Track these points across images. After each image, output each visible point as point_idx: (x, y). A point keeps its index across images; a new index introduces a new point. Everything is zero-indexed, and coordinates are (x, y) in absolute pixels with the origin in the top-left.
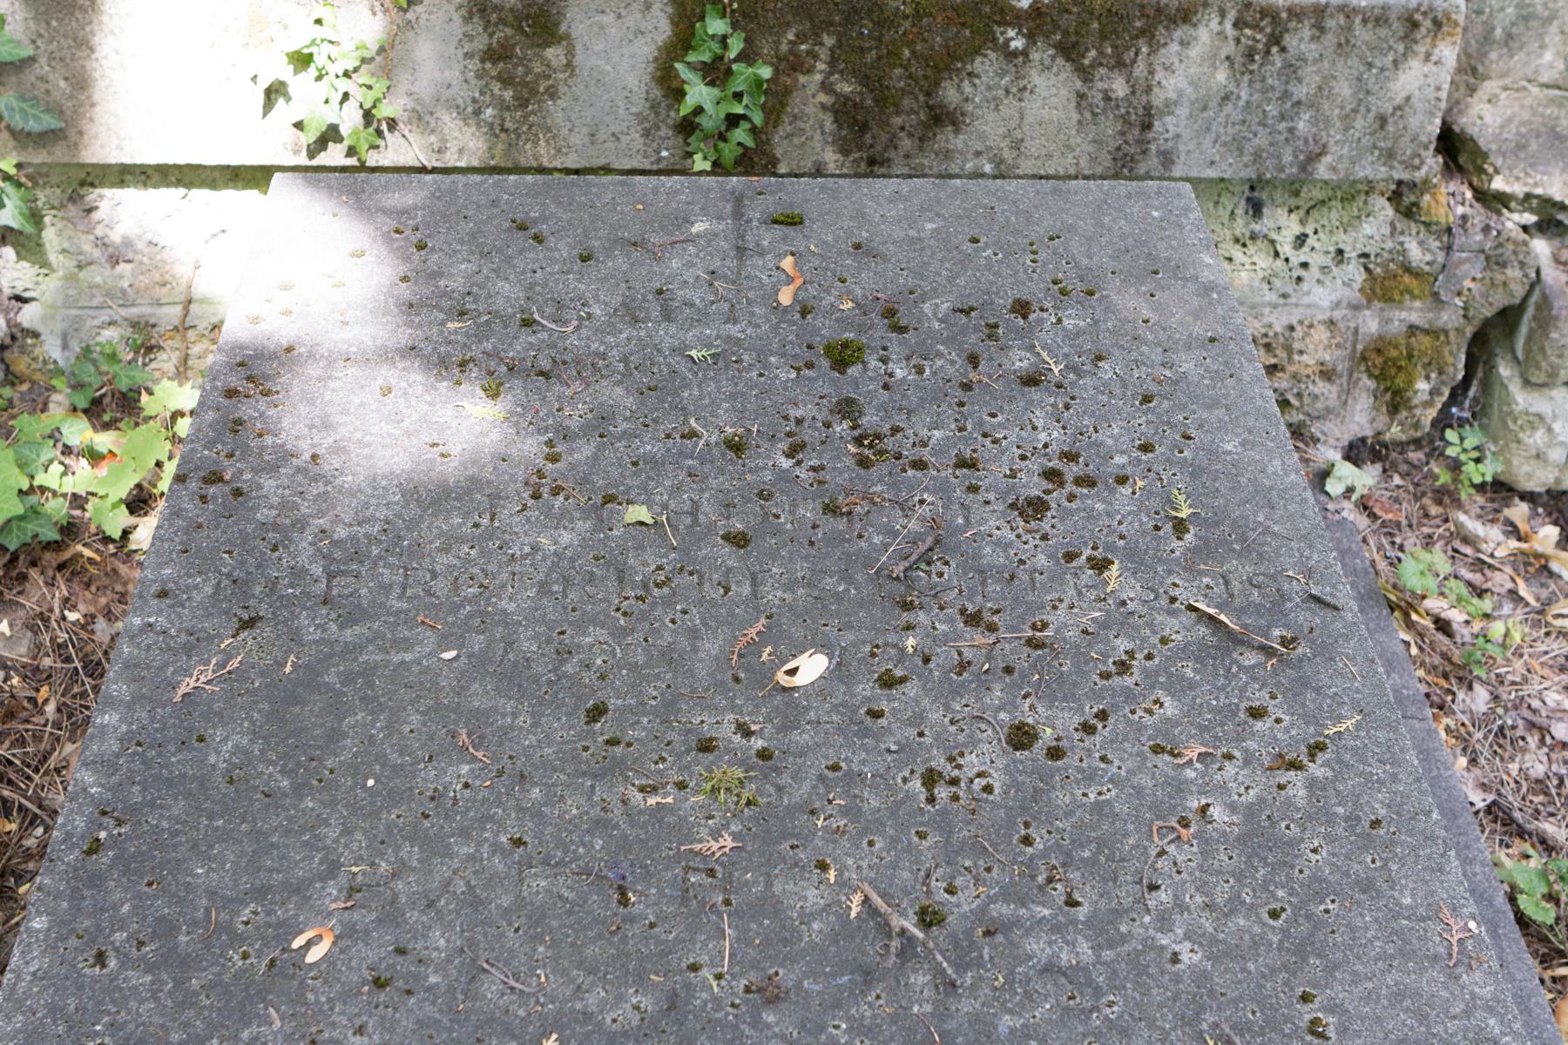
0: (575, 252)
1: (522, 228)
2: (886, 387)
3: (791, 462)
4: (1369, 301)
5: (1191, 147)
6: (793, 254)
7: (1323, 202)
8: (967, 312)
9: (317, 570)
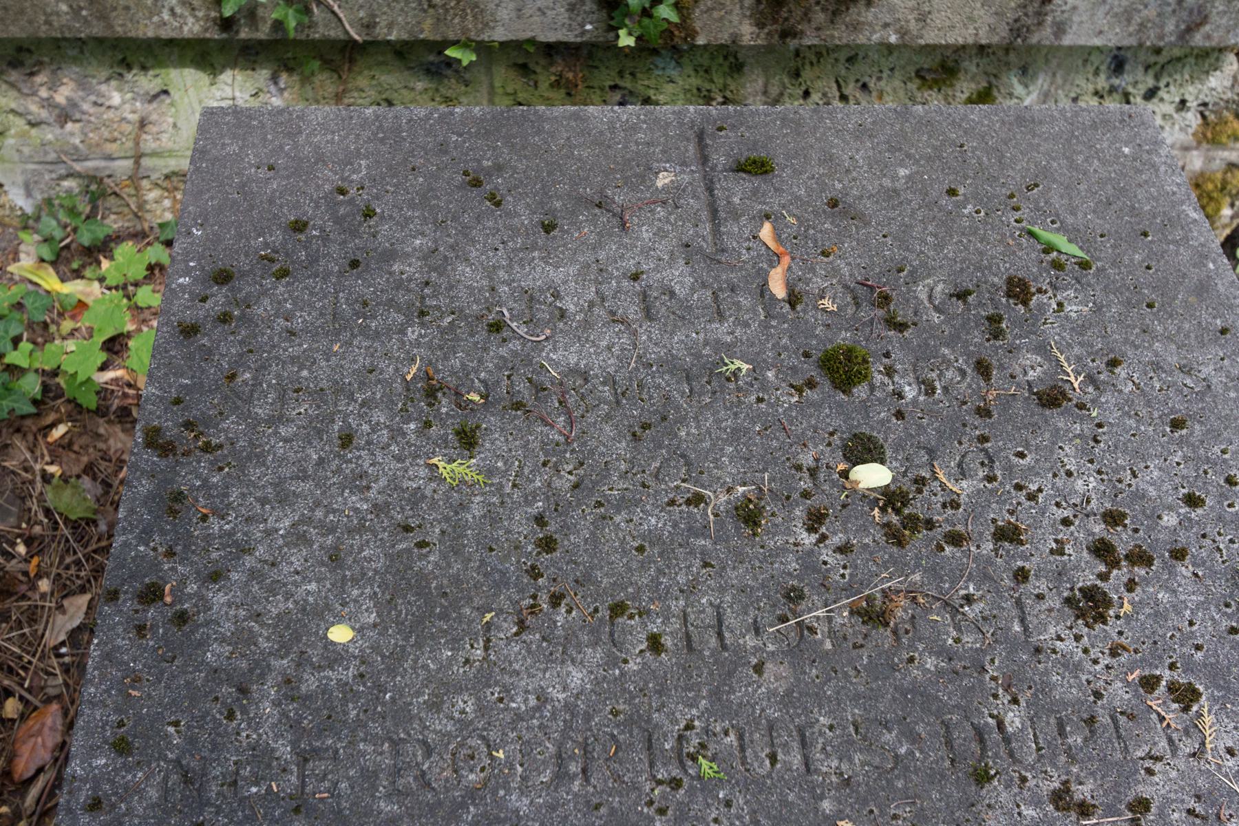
0: (536, 218)
1: (476, 183)
2: (899, 415)
3: (814, 537)
4: (1199, 143)
5: (1084, 18)
6: (768, 217)
7: (1179, 59)
8: (962, 295)
9: (284, 750)
